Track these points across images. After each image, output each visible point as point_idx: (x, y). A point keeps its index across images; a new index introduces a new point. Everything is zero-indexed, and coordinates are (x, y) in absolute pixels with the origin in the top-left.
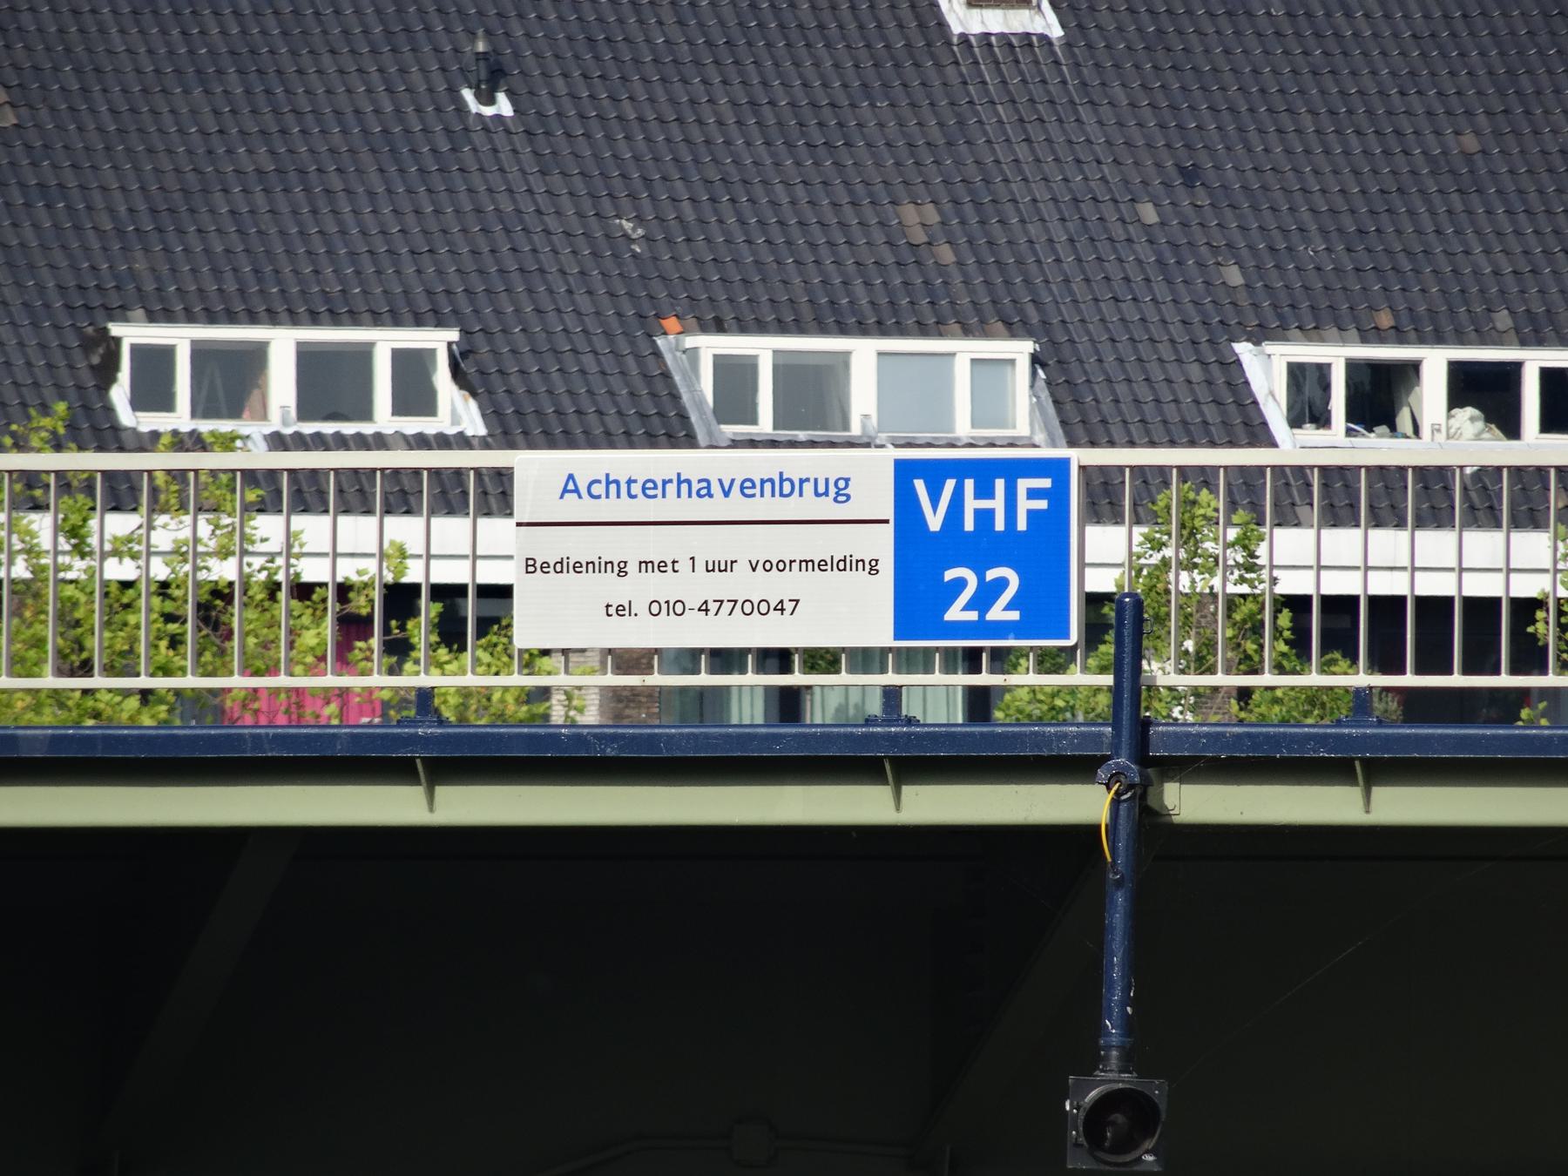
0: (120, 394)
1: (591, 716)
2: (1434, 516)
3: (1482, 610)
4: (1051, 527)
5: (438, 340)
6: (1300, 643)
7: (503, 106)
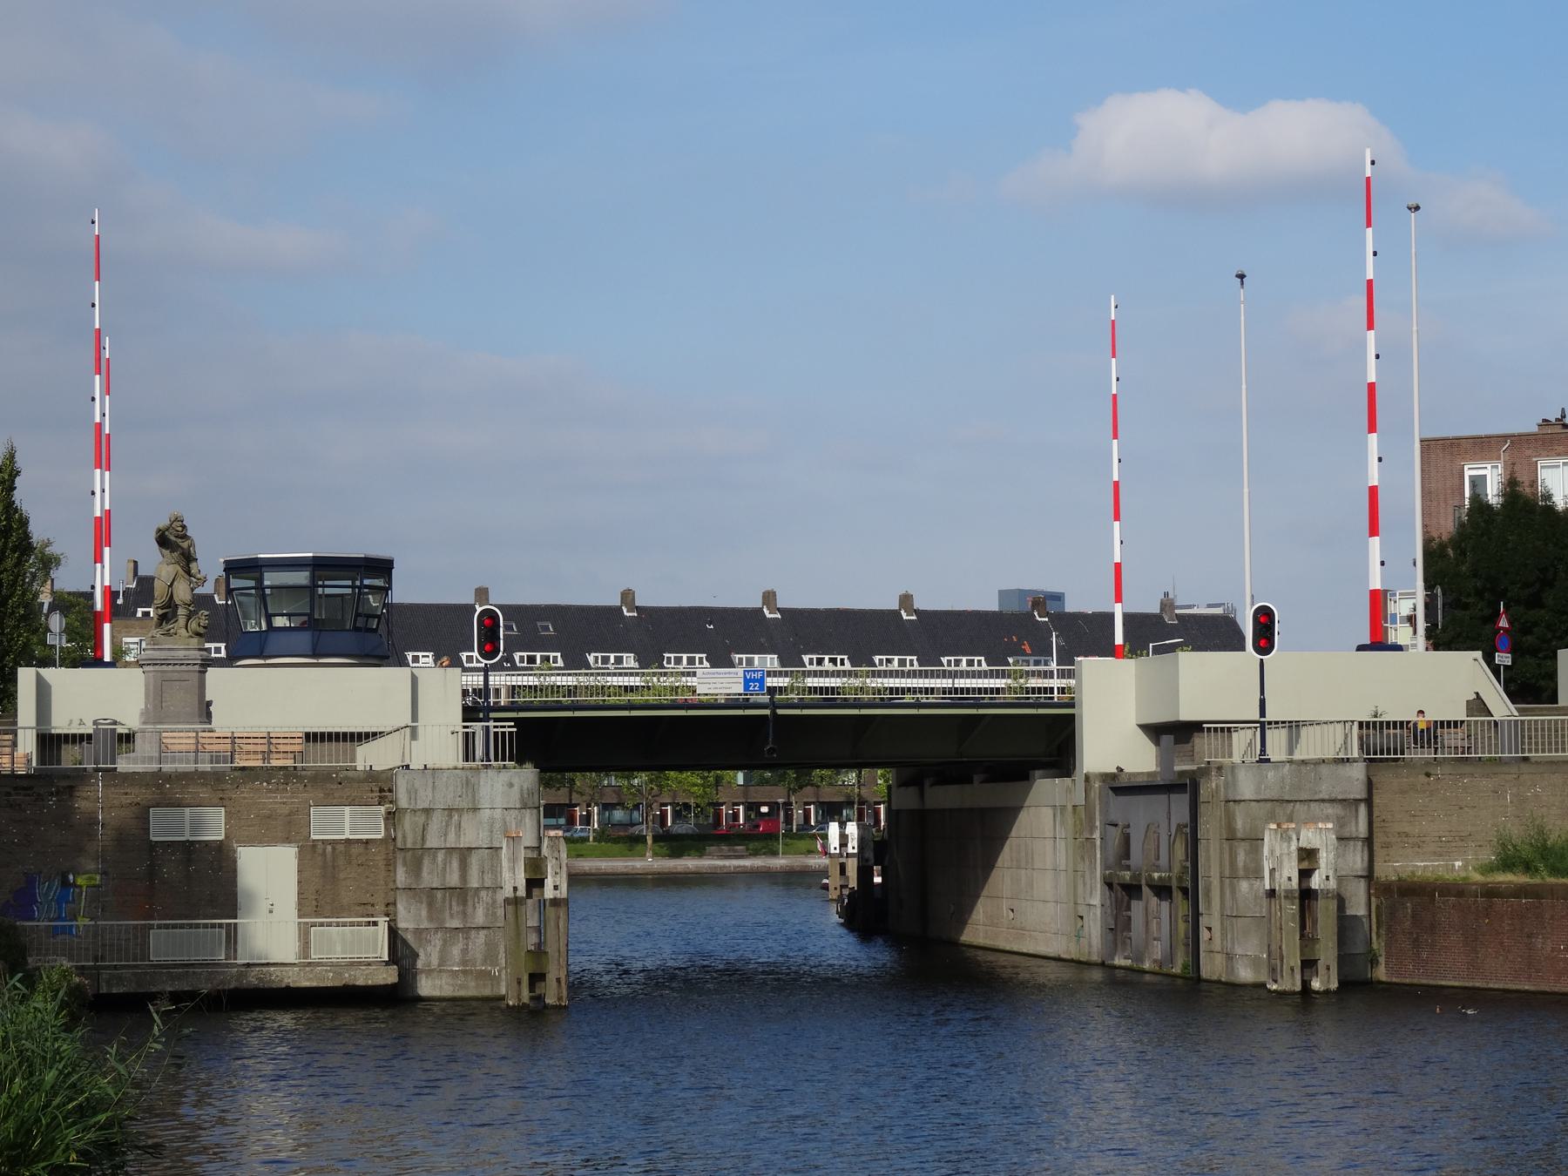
0: (665, 662)
1: (723, 701)
2: (827, 676)
3: (833, 688)
4: (762, 678)
5: (704, 655)
6: (552, 693)
7: (712, 627)
